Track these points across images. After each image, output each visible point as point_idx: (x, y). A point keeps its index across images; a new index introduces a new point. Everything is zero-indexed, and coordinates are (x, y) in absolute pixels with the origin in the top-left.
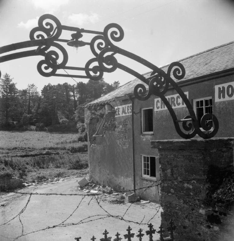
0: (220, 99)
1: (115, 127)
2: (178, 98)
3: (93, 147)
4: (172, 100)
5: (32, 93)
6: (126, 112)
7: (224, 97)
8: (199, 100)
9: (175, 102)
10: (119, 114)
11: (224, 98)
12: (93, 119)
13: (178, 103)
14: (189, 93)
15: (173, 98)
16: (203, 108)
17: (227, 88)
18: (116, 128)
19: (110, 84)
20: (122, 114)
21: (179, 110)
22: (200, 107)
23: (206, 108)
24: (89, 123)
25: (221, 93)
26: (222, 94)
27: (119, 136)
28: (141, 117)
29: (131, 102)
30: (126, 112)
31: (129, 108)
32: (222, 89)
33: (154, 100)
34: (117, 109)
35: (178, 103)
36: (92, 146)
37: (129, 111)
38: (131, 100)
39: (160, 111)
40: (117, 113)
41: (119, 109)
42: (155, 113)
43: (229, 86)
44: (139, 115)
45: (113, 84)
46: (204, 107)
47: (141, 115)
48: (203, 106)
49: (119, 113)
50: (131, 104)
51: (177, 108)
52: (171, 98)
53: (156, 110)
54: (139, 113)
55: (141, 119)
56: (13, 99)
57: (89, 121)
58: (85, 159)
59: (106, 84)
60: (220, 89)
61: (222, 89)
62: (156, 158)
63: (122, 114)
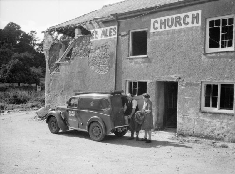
0: (193, 25)
1: (89, 52)
2: (156, 22)
3: (55, 75)
4: (177, 20)
5: (24, 97)
6: (108, 34)
7: (165, 27)
8: (214, 19)
9: (182, 22)
10: (96, 37)
11: (165, 28)
12: (55, 45)
13: (156, 27)
14: (202, 13)
15: (180, 18)
16: (219, 28)
17: (184, 18)
18: (90, 53)
19: (27, 33)
20: (101, 37)
21: (187, 30)
22: (215, 26)
23: (223, 28)
24: (49, 50)
25: (163, 24)
26: (163, 26)
27: (94, 61)
28: (129, 39)
29: (117, 23)
30: (108, 34)
31: (112, 30)
32: (163, 21)
33: (150, 21)
34: (93, 32)
35: (156, 27)
36: (54, 73)
37: (112, 34)
38: (117, 21)
39: (159, 32)
40: (94, 36)
41: (96, 32)
42: (152, 34)
43: (185, 15)
44: (126, 37)
45: (29, 32)
46: (221, 27)
47: (129, 37)
48: (220, 25)
49: (97, 36)
50: (116, 26)
51: (184, 28)
52: (176, 17)
53: (152, 30)
54: (126, 35)
55: (129, 42)
56: (16, 65)
57: (50, 47)
58: (61, 100)
59: (22, 32)
60: (162, 22)
61: (163, 21)
62: (148, 82)
63: (101, 37)
